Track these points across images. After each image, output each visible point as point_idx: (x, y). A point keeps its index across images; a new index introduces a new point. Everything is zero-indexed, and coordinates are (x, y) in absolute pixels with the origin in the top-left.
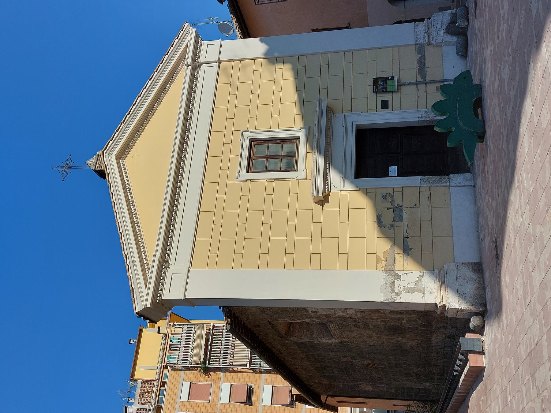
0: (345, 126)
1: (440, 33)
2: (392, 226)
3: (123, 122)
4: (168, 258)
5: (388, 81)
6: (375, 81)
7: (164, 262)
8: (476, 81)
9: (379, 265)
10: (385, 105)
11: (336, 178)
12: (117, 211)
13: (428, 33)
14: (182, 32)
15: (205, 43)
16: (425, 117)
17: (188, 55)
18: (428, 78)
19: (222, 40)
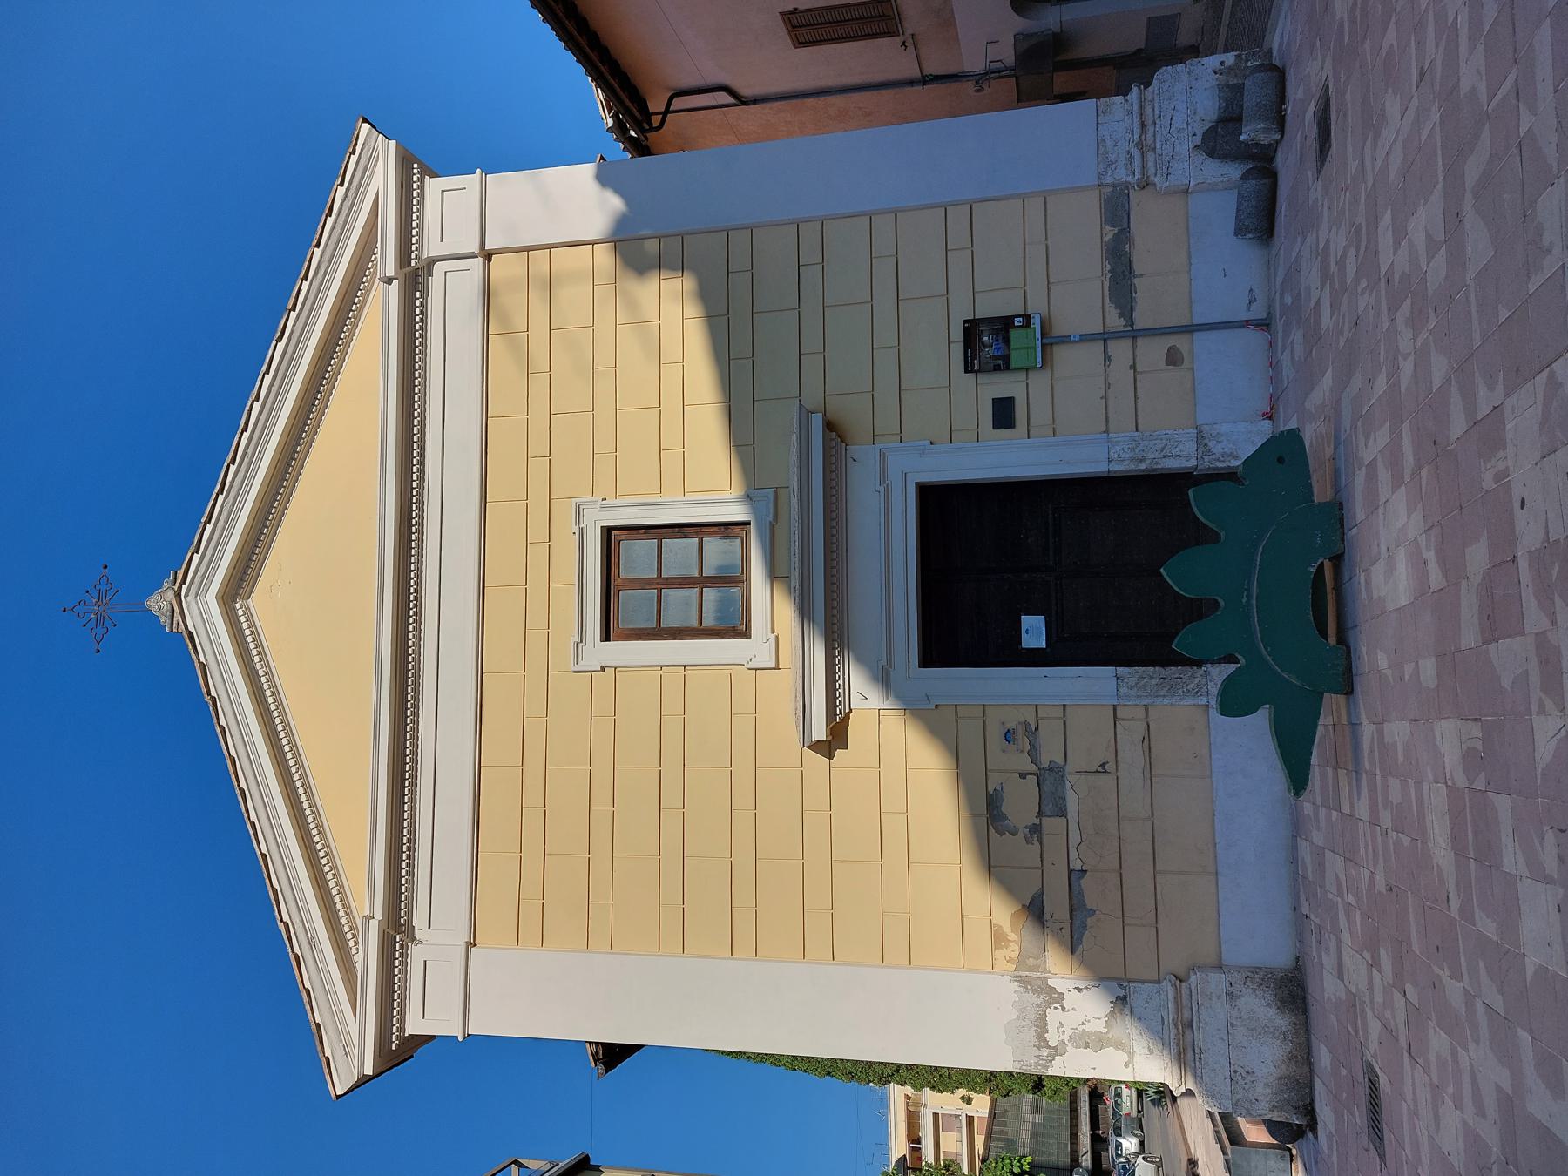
0: (882, 489)
1: (1184, 148)
2: (1036, 830)
3: (233, 461)
4: (409, 914)
5: (1013, 333)
6: (971, 330)
7: (397, 930)
8: (1321, 492)
9: (998, 953)
10: (1004, 413)
11: (864, 697)
12: (243, 785)
13: (1140, 145)
14: (354, 159)
15: (433, 186)
16: (1132, 459)
17: (384, 257)
18: (1142, 320)
19: (486, 172)
